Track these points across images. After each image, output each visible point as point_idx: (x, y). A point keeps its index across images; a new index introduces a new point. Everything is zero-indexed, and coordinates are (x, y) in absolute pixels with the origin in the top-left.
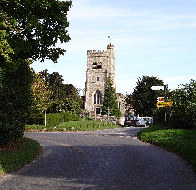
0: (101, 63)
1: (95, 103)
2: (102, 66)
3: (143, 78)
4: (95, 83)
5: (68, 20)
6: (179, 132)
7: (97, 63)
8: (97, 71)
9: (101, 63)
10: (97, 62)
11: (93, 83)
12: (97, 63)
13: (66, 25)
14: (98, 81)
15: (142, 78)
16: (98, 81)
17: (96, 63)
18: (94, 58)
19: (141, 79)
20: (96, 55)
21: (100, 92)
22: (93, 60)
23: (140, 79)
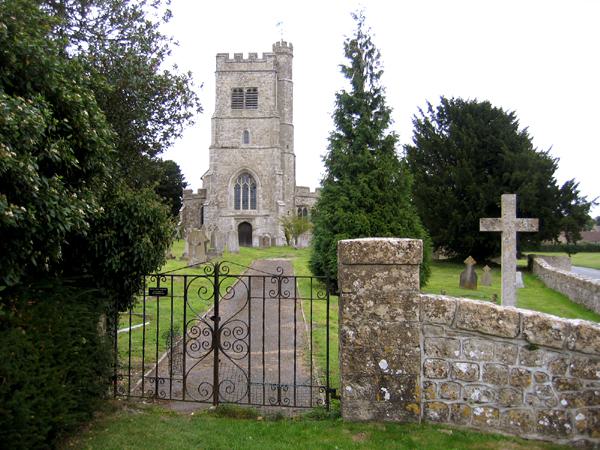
0: (255, 89)
1: (237, 207)
2: (260, 100)
3: (439, 104)
4: (236, 148)
5: (539, 145)
6: (311, 172)
7: (245, 91)
8: (245, 113)
9: (255, 89)
10: (245, 87)
11: (233, 148)
12: (245, 91)
13: (547, 166)
14: (247, 142)
15: (437, 103)
16: (247, 142)
17: (241, 90)
18: (235, 74)
19: (434, 108)
20: (243, 67)
21: (251, 176)
22: (232, 82)
23: (430, 109)
